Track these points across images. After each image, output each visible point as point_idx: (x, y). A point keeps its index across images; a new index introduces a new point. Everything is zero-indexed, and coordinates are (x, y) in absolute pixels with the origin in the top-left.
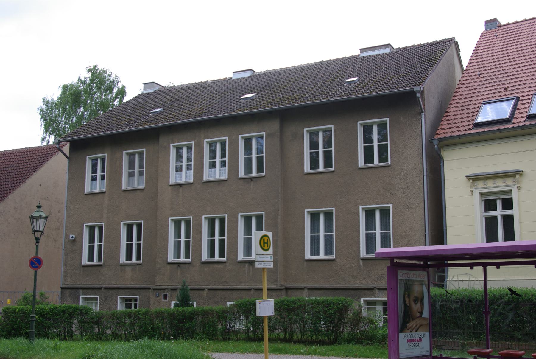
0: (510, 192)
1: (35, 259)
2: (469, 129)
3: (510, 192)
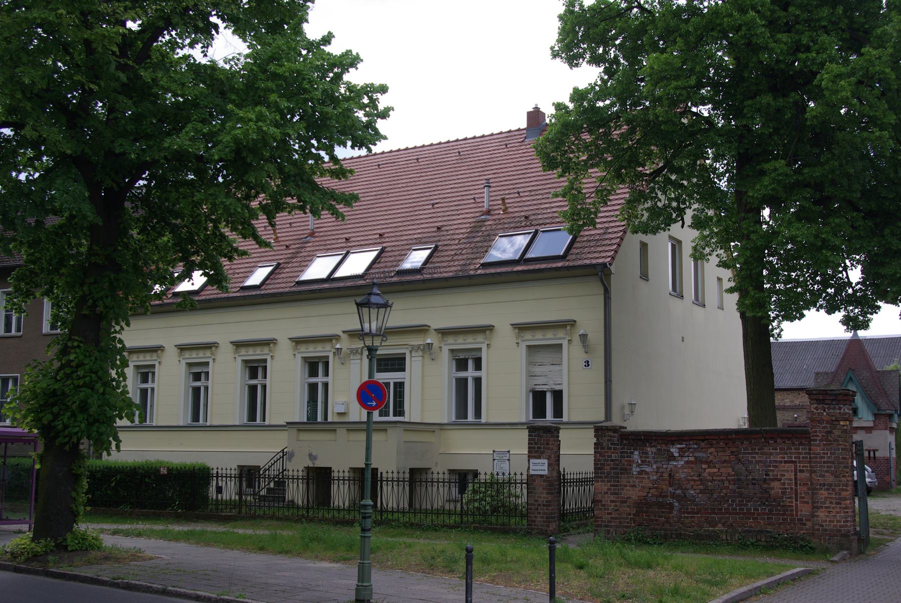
0: (480, 349)
1: (374, 404)
2: (291, 287)
3: (480, 349)
